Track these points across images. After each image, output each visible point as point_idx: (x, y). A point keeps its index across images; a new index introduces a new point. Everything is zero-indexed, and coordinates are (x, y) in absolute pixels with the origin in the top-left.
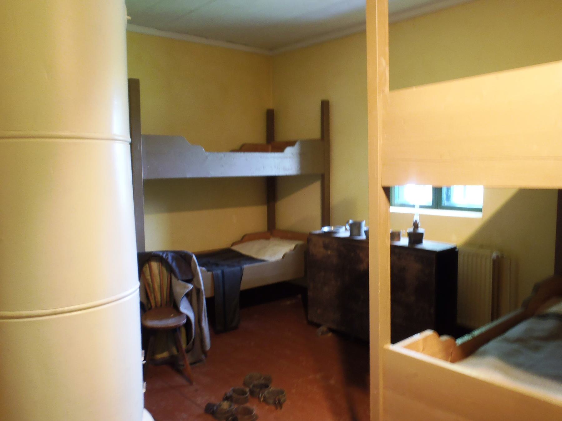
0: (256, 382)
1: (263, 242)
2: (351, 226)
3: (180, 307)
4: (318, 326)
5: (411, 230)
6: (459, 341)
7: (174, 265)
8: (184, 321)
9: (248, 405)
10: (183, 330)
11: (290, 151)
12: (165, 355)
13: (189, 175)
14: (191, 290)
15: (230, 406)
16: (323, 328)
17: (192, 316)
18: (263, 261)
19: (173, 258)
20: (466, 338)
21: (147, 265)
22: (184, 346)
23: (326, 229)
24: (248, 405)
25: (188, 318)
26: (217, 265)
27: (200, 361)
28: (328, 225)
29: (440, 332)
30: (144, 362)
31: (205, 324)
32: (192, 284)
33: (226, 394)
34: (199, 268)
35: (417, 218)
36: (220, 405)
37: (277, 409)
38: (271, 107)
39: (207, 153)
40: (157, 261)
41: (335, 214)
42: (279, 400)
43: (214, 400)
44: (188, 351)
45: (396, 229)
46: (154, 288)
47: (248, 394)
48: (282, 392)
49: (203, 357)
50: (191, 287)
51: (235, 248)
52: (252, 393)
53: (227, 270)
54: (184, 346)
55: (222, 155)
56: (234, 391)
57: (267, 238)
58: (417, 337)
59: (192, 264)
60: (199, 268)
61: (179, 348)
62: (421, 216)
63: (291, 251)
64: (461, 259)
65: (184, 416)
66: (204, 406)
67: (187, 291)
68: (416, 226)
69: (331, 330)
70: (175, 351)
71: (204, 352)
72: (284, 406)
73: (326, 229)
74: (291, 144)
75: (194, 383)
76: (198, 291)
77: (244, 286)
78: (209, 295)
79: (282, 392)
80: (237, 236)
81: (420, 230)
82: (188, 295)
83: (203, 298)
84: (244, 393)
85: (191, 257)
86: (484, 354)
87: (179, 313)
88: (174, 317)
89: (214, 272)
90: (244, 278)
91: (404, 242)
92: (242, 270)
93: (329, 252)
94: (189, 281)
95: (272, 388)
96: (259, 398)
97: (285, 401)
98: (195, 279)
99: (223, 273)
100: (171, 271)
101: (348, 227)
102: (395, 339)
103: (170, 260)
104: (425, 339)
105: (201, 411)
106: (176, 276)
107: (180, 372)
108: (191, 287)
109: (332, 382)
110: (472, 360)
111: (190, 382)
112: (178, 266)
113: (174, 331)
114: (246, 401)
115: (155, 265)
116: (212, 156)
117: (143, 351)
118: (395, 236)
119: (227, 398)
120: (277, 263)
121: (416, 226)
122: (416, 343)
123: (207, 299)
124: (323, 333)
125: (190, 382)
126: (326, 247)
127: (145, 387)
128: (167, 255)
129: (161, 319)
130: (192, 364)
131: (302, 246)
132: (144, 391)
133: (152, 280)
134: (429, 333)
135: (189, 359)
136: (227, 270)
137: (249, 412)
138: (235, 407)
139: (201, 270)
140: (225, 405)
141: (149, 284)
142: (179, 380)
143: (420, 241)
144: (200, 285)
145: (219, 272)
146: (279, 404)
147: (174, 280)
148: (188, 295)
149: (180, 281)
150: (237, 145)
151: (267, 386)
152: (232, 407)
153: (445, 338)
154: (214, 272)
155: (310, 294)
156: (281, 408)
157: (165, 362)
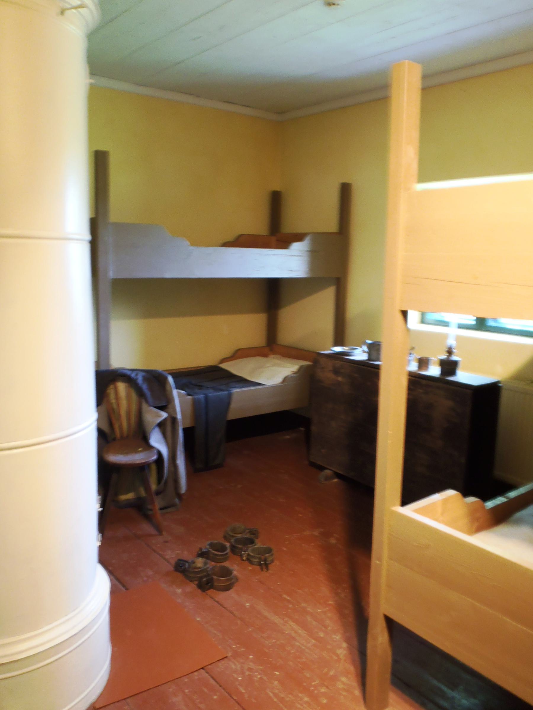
0: (239, 536)
1: (260, 360)
2: (370, 346)
3: (149, 439)
4: (322, 468)
5: (444, 357)
6: (490, 504)
7: (145, 387)
8: (155, 457)
9: (227, 564)
10: (154, 467)
11: (296, 247)
12: (130, 496)
13: (168, 276)
14: (165, 420)
15: (205, 564)
16: (327, 472)
17: (164, 451)
18: (259, 384)
19: (145, 379)
20: (500, 500)
21: (112, 387)
22: (154, 487)
23: (338, 349)
24: (227, 564)
25: (160, 454)
26: (200, 387)
27: (173, 505)
28: (342, 344)
29: (465, 493)
30: (101, 509)
31: (181, 462)
32: (166, 412)
33: (201, 549)
34: (175, 393)
35: (451, 342)
36: (194, 562)
37: (262, 570)
38: (277, 189)
39: (192, 248)
40: (123, 381)
41: (353, 329)
42: (265, 560)
43: (186, 555)
44: (158, 493)
45: (424, 355)
46: (120, 416)
47: (228, 551)
48: (269, 551)
49: (177, 501)
50: (164, 415)
51: (224, 366)
52: (233, 549)
53: (212, 394)
54: (154, 487)
55: (210, 250)
56: (211, 545)
57: (265, 356)
58: (436, 498)
59: (168, 388)
60: (175, 393)
61: (147, 488)
62: (458, 338)
63: (295, 373)
64: (505, 399)
65: (150, 573)
66: (173, 562)
67: (160, 420)
68: (450, 352)
69: (338, 475)
70: (143, 493)
71: (179, 496)
72: (271, 567)
73: (338, 349)
74: (299, 237)
75: (164, 533)
76: (173, 420)
77: (232, 415)
78: (188, 425)
79: (269, 551)
80: (227, 352)
81: (454, 358)
82: (161, 425)
83: (178, 430)
84: (223, 548)
85: (166, 378)
86: (519, 522)
87: (151, 447)
88: (141, 451)
89: (197, 397)
90: (233, 405)
91: (434, 371)
92: (230, 396)
93: (340, 379)
94: (162, 408)
95: (259, 544)
96: (241, 556)
97: (272, 561)
98: (170, 406)
99: (206, 398)
100: (141, 394)
101: (365, 348)
102: (405, 501)
103: (140, 380)
104: (445, 501)
105: (171, 568)
106: (147, 402)
107: (148, 517)
108: (164, 415)
109: (333, 541)
110: (503, 529)
111: (160, 531)
112: (151, 389)
113: (142, 468)
114: (225, 558)
115: (121, 386)
116: (198, 252)
117: (100, 497)
118: (423, 363)
119: (202, 554)
120: (274, 387)
121: (450, 352)
122: (434, 504)
123: (185, 430)
124: (327, 478)
125: (160, 531)
126: (336, 371)
127: (100, 540)
128: (137, 375)
129: (127, 453)
130: (161, 509)
131: (308, 367)
132: (99, 544)
133: (118, 404)
134: (451, 493)
135: (158, 503)
136: (212, 394)
137: (227, 573)
138: (211, 565)
139: (179, 395)
140: (200, 562)
141: (113, 409)
142: (147, 528)
143: (453, 373)
144: (176, 413)
145: (201, 396)
146: (265, 565)
147: (145, 406)
148: (161, 425)
149: (152, 408)
150: (230, 238)
151: (252, 542)
152: (208, 566)
153: (472, 499)
154: (197, 397)
155: (314, 428)
156: (267, 569)
157: (130, 504)
